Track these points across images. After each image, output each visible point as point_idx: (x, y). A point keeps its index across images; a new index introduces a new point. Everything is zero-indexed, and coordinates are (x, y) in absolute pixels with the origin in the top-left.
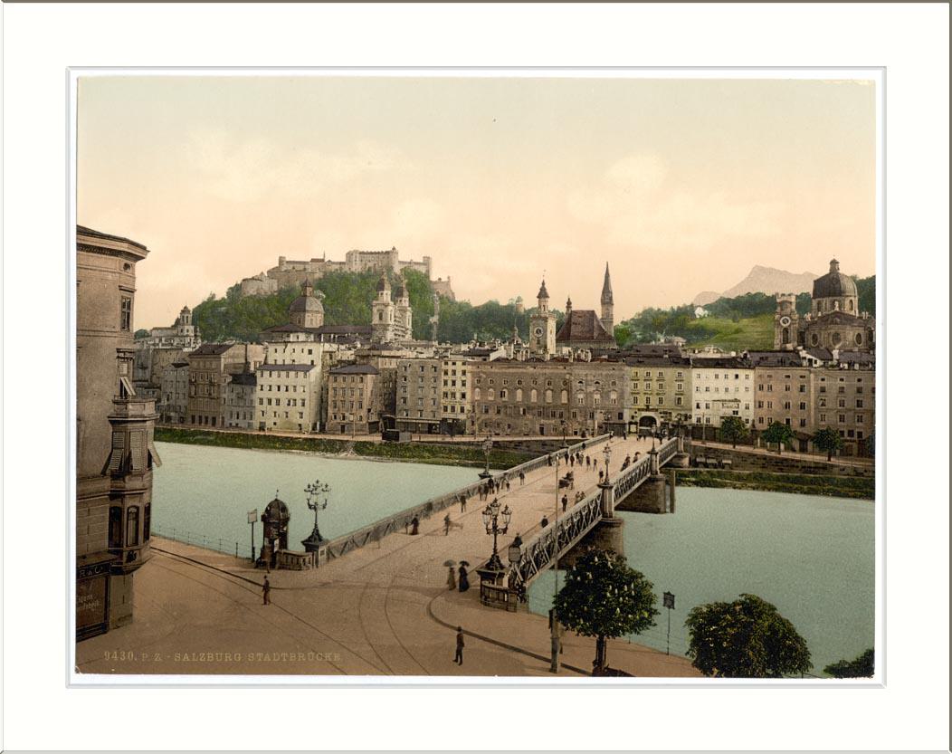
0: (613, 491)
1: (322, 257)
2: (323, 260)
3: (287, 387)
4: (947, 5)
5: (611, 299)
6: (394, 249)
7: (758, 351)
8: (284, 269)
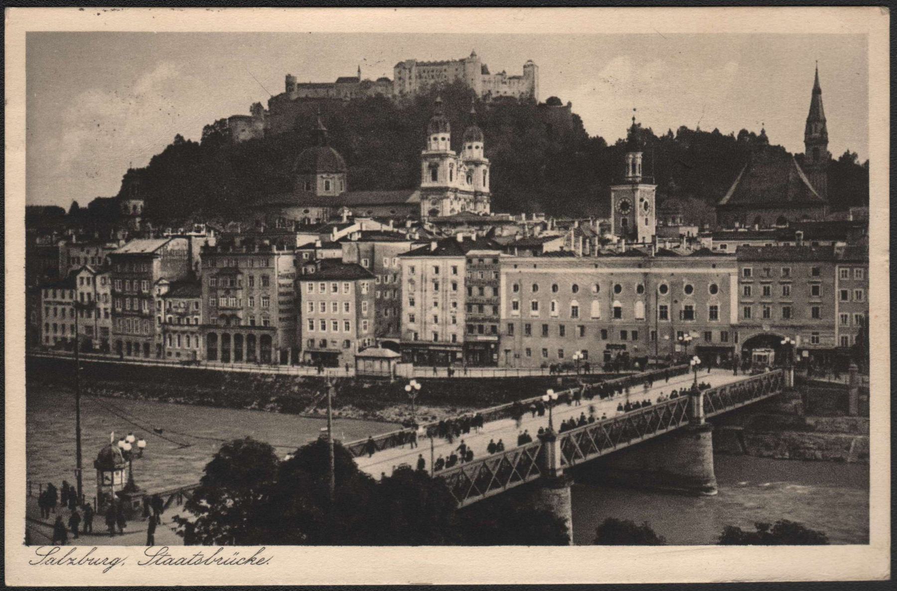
0: (558, 444)
1: (355, 75)
2: (356, 80)
3: (323, 322)
4: (9, 582)
5: (824, 132)
6: (473, 55)
7: (287, 447)
8: (294, 97)
